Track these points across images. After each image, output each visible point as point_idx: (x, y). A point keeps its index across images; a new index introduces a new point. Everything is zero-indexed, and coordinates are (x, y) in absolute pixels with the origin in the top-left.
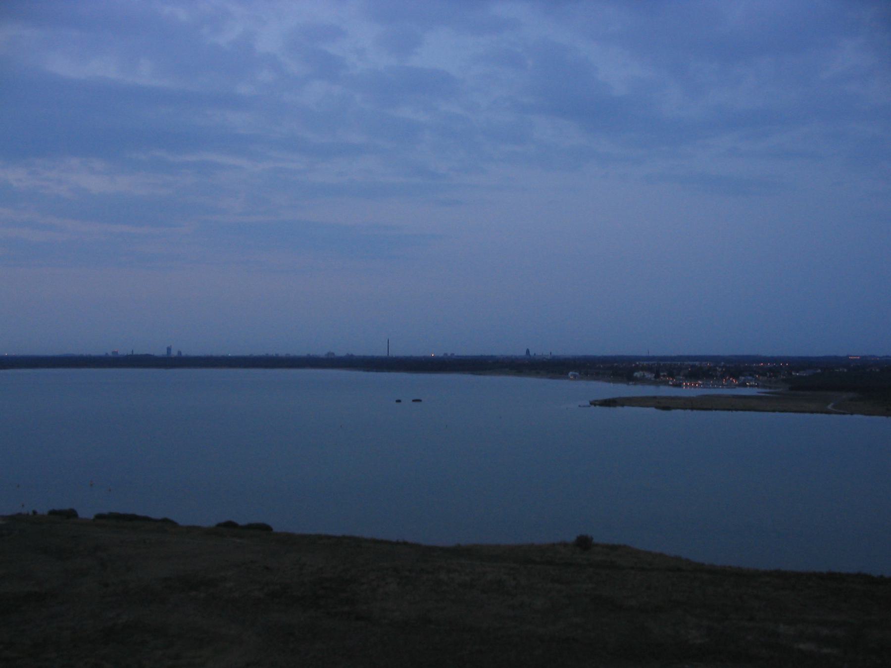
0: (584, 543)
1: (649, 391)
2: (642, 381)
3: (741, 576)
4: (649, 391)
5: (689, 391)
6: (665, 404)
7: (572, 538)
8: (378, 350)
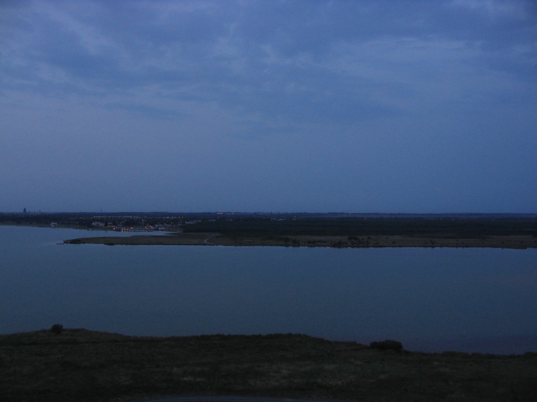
0: (57, 329)
1: (101, 234)
2: (97, 228)
3: (152, 342)
4: (101, 234)
5: (125, 233)
6: (110, 242)
7: (49, 327)
8: (16, 209)
